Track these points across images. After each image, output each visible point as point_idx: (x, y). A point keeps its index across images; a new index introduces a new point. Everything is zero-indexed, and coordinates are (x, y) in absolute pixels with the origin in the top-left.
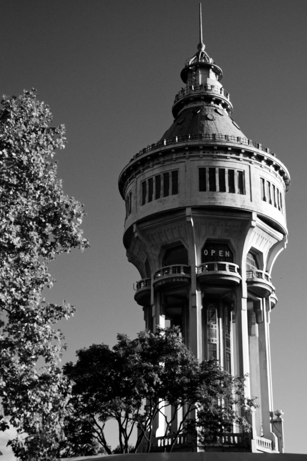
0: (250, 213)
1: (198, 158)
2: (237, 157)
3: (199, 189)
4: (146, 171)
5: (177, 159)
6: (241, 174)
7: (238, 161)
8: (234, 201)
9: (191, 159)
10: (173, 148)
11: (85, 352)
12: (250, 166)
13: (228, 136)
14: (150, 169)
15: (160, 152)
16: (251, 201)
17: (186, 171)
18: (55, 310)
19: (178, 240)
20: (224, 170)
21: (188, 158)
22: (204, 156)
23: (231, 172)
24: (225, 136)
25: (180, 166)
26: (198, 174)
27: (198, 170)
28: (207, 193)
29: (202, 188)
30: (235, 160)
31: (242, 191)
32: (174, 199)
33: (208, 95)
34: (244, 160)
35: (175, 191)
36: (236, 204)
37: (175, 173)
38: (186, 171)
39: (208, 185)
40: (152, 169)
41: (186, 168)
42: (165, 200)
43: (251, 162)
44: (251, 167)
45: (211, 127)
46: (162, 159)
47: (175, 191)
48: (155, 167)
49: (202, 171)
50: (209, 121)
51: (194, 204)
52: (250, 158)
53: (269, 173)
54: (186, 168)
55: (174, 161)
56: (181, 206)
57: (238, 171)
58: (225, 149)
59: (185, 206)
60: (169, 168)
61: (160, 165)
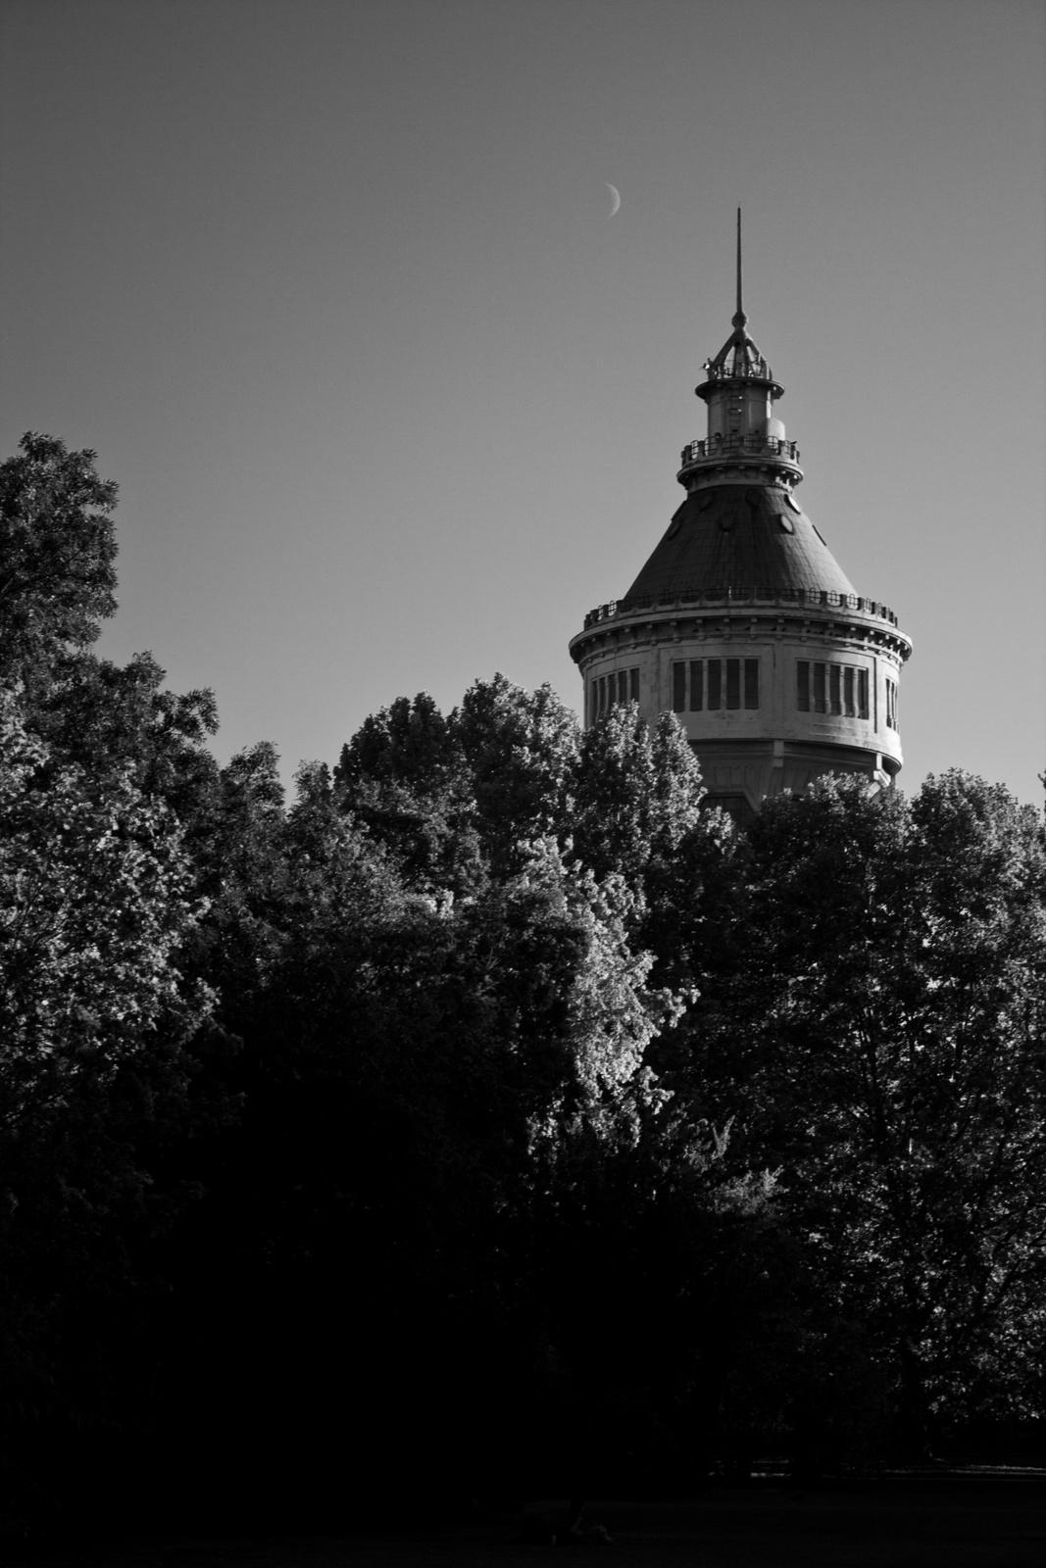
0: (872, 755)
1: (797, 642)
2: (861, 643)
3: (759, 665)
4: (684, 643)
5: (757, 637)
6: (864, 674)
7: (861, 652)
8: (854, 735)
9: (785, 641)
10: (756, 616)
11: (401, 817)
12: (875, 659)
13: (846, 597)
14: (696, 642)
15: (728, 617)
16: (876, 732)
17: (775, 664)
18: (486, 877)
19: (740, 790)
20: (839, 667)
21: (780, 640)
22: (809, 638)
23: (850, 671)
24: (841, 596)
25: (763, 653)
26: (796, 674)
27: (795, 667)
28: (811, 716)
29: (804, 706)
30: (855, 650)
31: (864, 716)
32: (751, 719)
33: (776, 465)
34: (870, 648)
35: (753, 701)
36: (857, 741)
37: (752, 665)
38: (775, 664)
39: (812, 700)
40: (702, 643)
41: (774, 659)
42: (731, 716)
43: (877, 652)
44: (877, 660)
45: (797, 556)
46: (727, 631)
47: (753, 701)
48: (710, 641)
49: (803, 667)
50: (787, 535)
51: (789, 736)
52: (877, 643)
53: (888, 660)
54: (774, 659)
55: (752, 639)
56: (766, 735)
57: (859, 671)
58: (844, 628)
59: (773, 736)
60: (743, 651)
61: (720, 640)
